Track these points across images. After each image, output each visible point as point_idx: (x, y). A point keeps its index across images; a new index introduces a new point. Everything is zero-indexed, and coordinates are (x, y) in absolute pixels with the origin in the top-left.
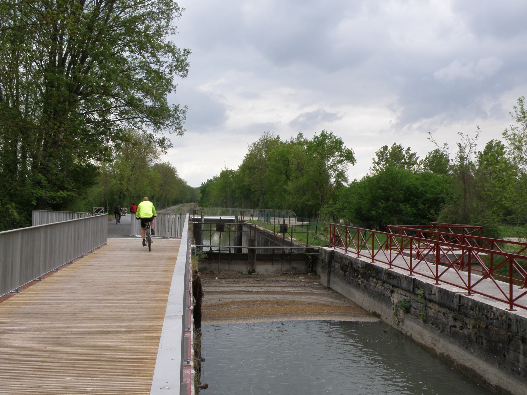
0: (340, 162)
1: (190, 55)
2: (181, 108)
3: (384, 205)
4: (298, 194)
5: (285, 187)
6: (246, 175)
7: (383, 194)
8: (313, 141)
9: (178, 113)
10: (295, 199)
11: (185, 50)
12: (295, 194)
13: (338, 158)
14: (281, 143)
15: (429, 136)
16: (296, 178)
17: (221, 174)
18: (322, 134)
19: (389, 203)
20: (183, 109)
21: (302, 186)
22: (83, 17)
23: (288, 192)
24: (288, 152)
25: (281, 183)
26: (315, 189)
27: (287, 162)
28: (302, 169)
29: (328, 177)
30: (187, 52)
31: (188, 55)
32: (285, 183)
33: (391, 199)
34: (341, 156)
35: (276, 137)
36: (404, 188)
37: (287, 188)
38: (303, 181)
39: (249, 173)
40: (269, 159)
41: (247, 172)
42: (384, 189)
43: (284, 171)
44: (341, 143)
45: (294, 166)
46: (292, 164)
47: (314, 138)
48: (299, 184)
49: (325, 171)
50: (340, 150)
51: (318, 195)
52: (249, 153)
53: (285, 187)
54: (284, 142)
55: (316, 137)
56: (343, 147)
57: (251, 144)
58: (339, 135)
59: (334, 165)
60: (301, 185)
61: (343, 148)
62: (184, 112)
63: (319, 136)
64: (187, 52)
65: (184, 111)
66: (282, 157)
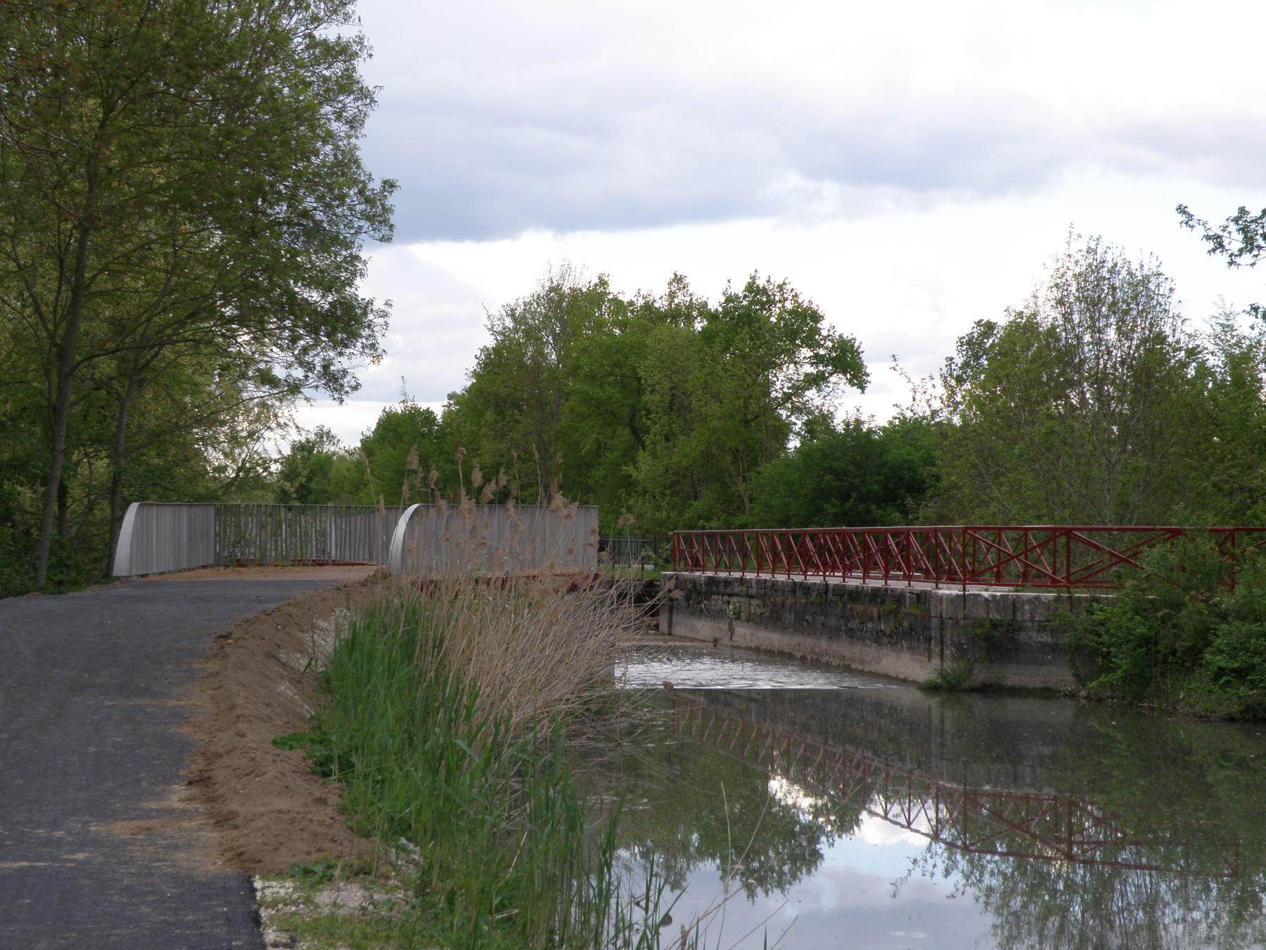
0: (816, 381)
1: (396, 193)
2: (378, 305)
3: (835, 510)
4: (673, 494)
5: (630, 470)
6: (484, 430)
7: (838, 483)
8: (720, 309)
9: (371, 317)
10: (665, 513)
11: (385, 182)
12: (663, 495)
13: (808, 369)
14: (616, 302)
15: (893, 364)
16: (667, 440)
17: (379, 425)
18: (751, 288)
19: (848, 505)
20: (383, 307)
21: (687, 469)
22: (650, 558)
23: (640, 488)
24: (638, 349)
25: (610, 456)
26: (731, 476)
27: (633, 385)
28: (687, 408)
29: (782, 431)
30: (389, 185)
31: (391, 192)
32: (629, 457)
33: (854, 495)
34: (817, 360)
35: (596, 280)
36: (886, 470)
37: (635, 474)
38: (689, 448)
39: (496, 422)
40: (573, 372)
41: (490, 415)
42: (839, 471)
43: (625, 412)
44: (816, 317)
45: (657, 397)
46: (652, 392)
47: (723, 299)
48: (675, 459)
49: (768, 410)
50: (811, 340)
51: (740, 496)
52: (490, 342)
53: (630, 470)
54: (625, 299)
55: (729, 299)
56: (824, 326)
57: (497, 310)
58: (810, 293)
59: (796, 394)
60: (685, 463)
61: (824, 333)
62: (384, 314)
63: (741, 295)
64: (389, 185)
65: (383, 311)
66: (617, 365)
